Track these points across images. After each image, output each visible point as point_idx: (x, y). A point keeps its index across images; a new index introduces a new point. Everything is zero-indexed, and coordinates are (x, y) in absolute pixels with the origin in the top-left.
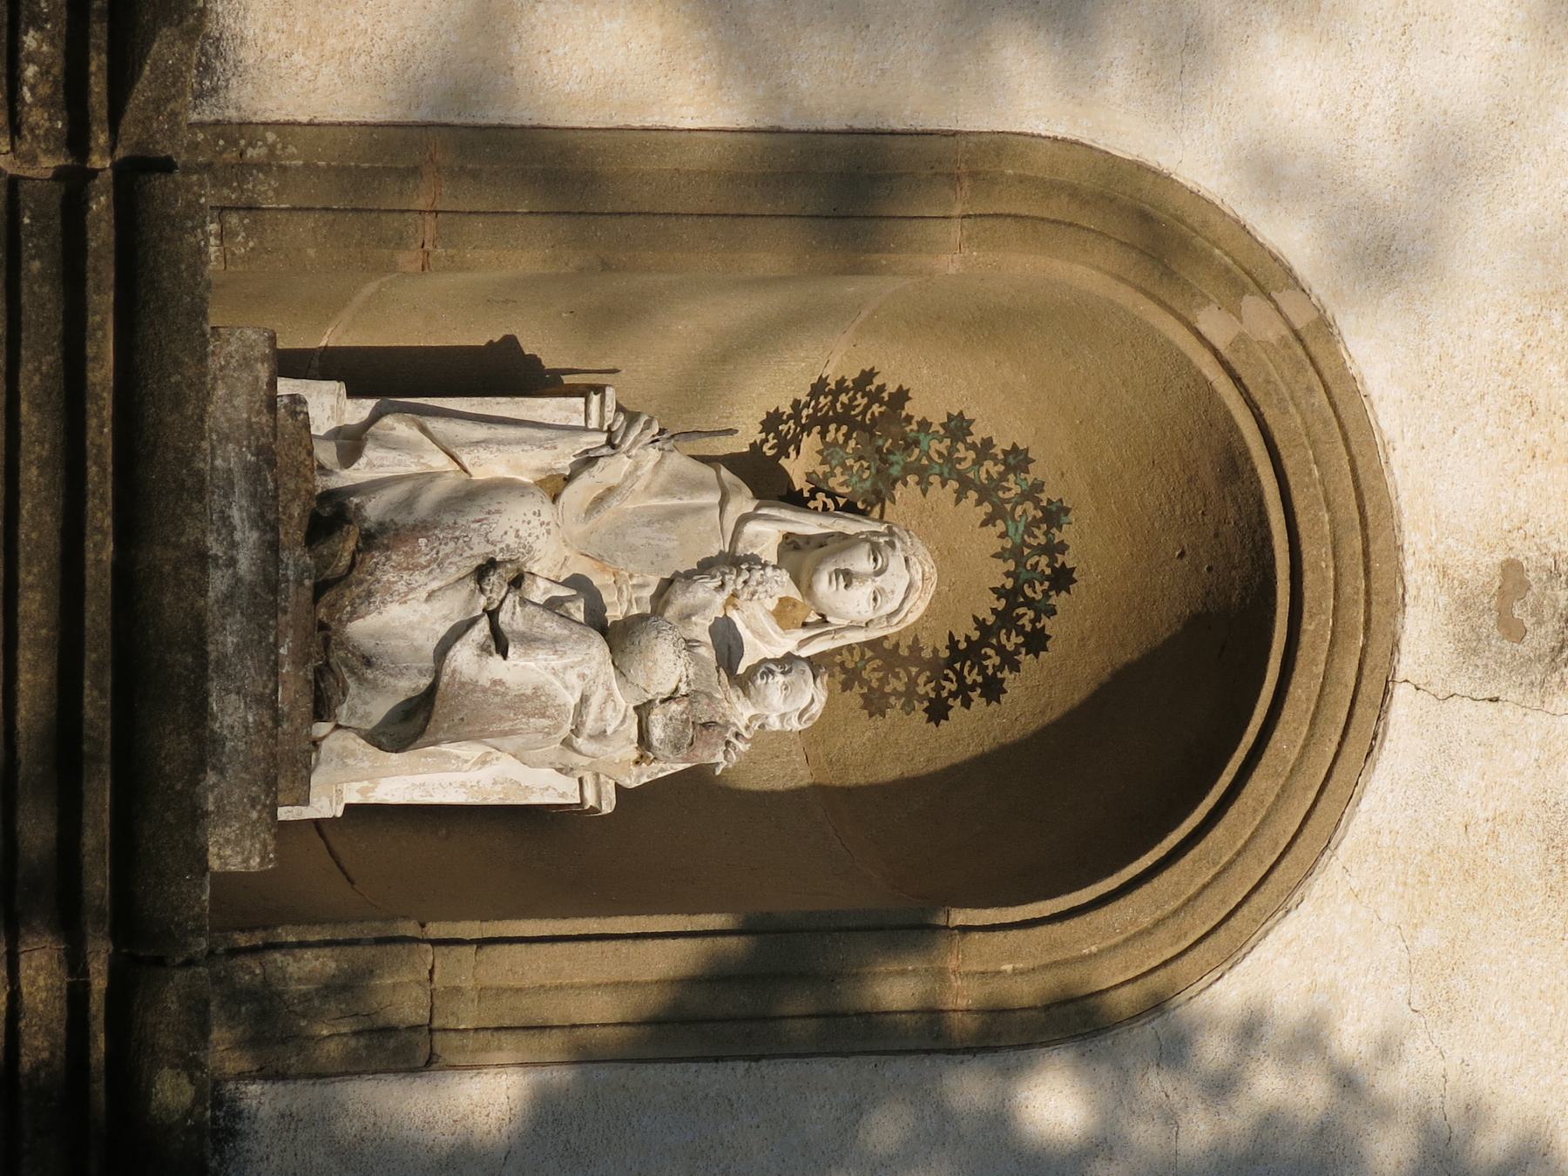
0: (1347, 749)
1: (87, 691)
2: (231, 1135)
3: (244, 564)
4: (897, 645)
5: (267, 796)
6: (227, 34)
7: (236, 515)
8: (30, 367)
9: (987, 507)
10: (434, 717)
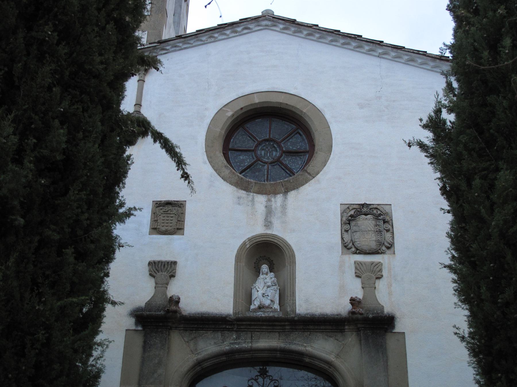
3: (262, 313)
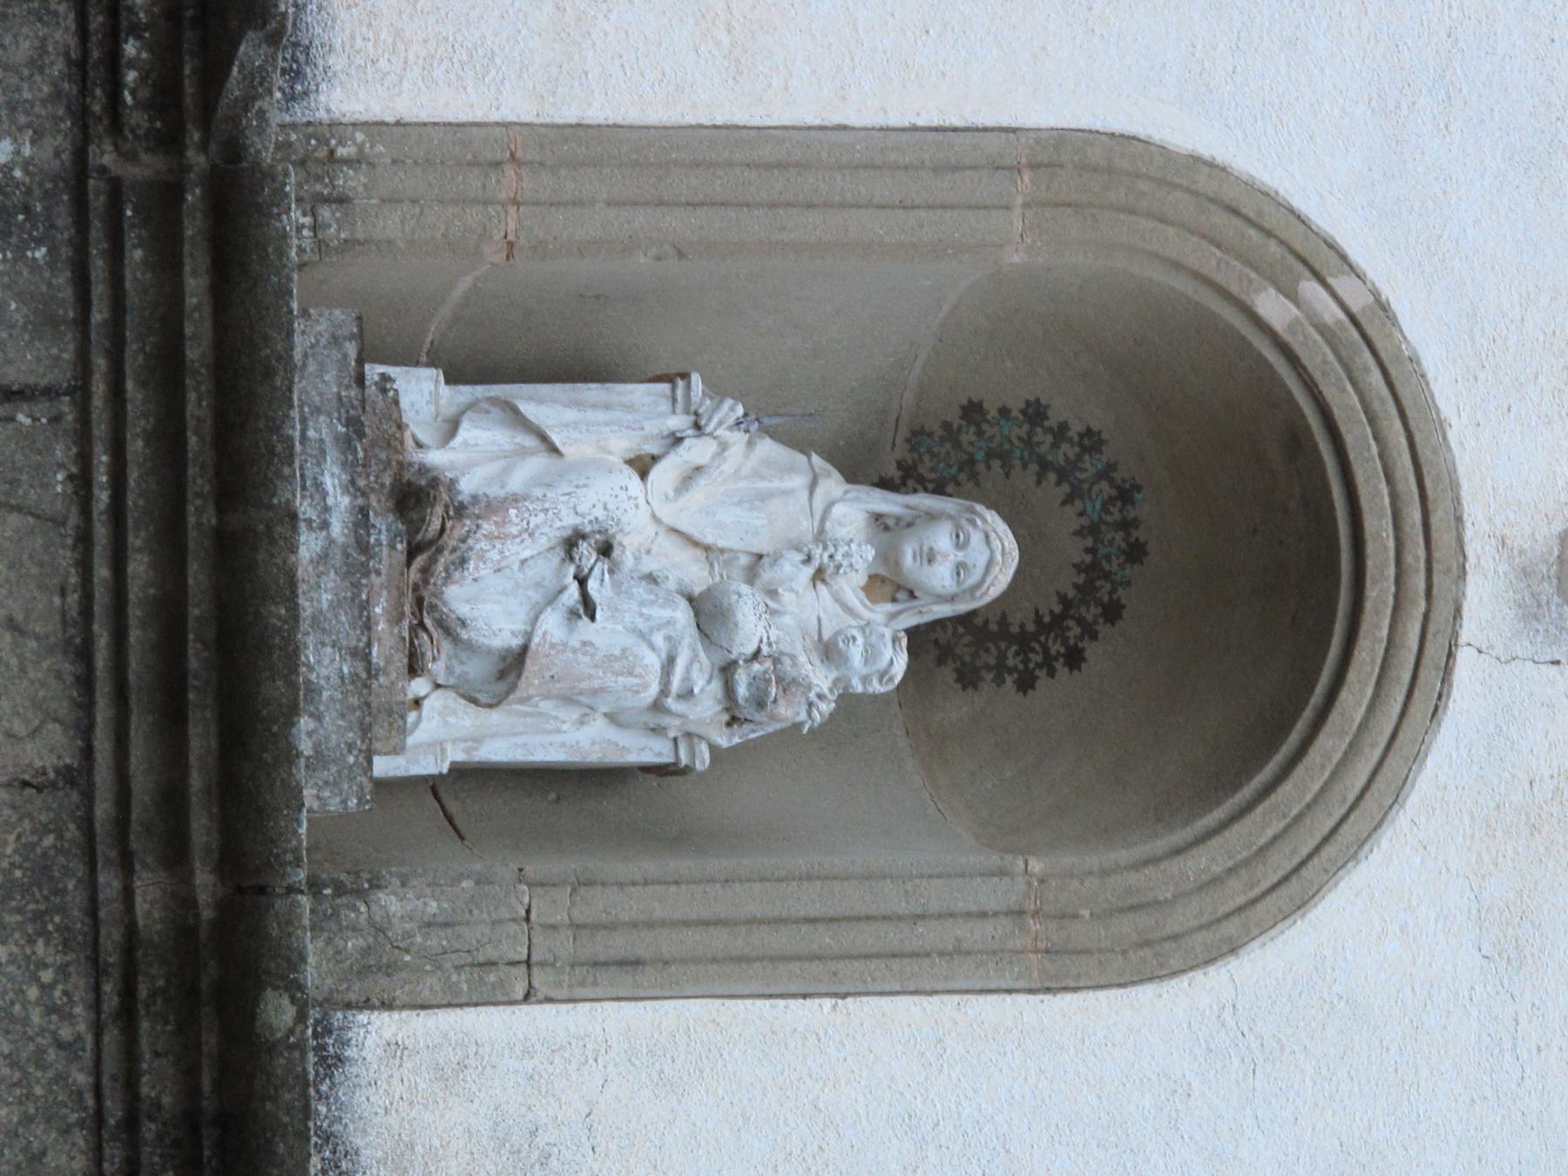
0: (1412, 709)
1: (191, 644)
2: (340, 1060)
3: (337, 529)
4: (986, 622)
5: (363, 742)
6: (317, 42)
7: (329, 482)
8: (135, 347)
9: (1066, 488)
10: (525, 674)
